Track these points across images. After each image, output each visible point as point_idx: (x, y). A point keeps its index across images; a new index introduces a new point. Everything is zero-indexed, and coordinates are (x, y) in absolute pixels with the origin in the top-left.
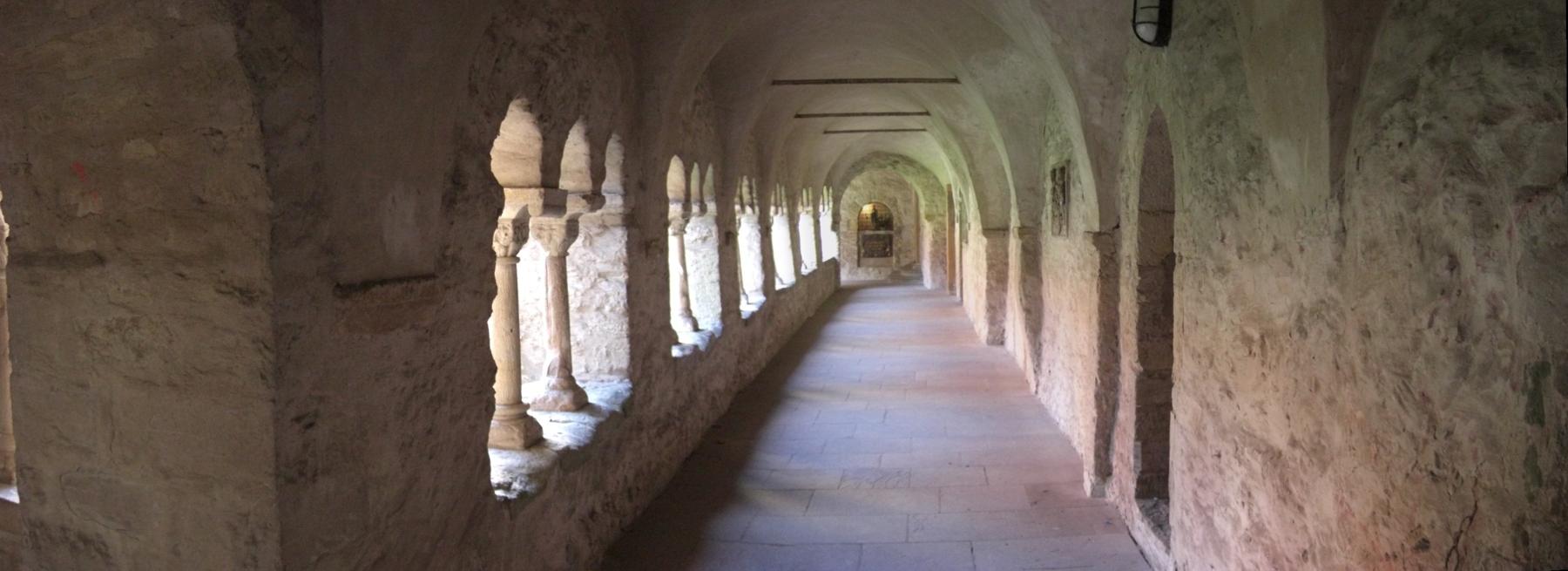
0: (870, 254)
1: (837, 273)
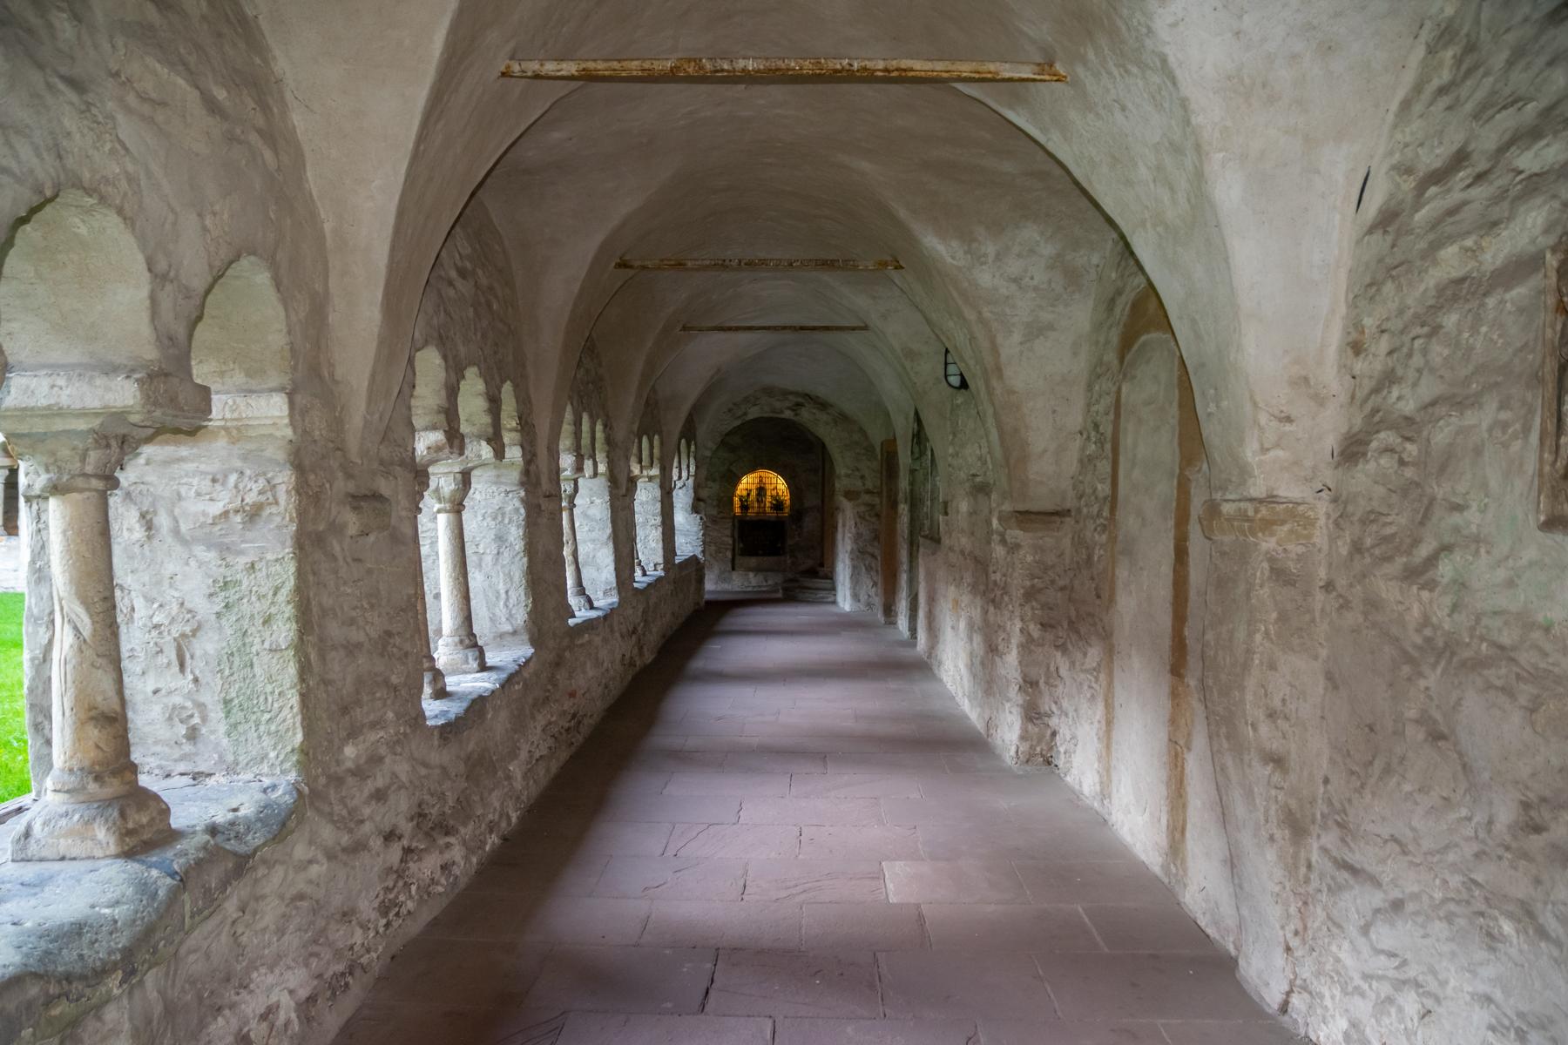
0: (747, 552)
1: (701, 580)
